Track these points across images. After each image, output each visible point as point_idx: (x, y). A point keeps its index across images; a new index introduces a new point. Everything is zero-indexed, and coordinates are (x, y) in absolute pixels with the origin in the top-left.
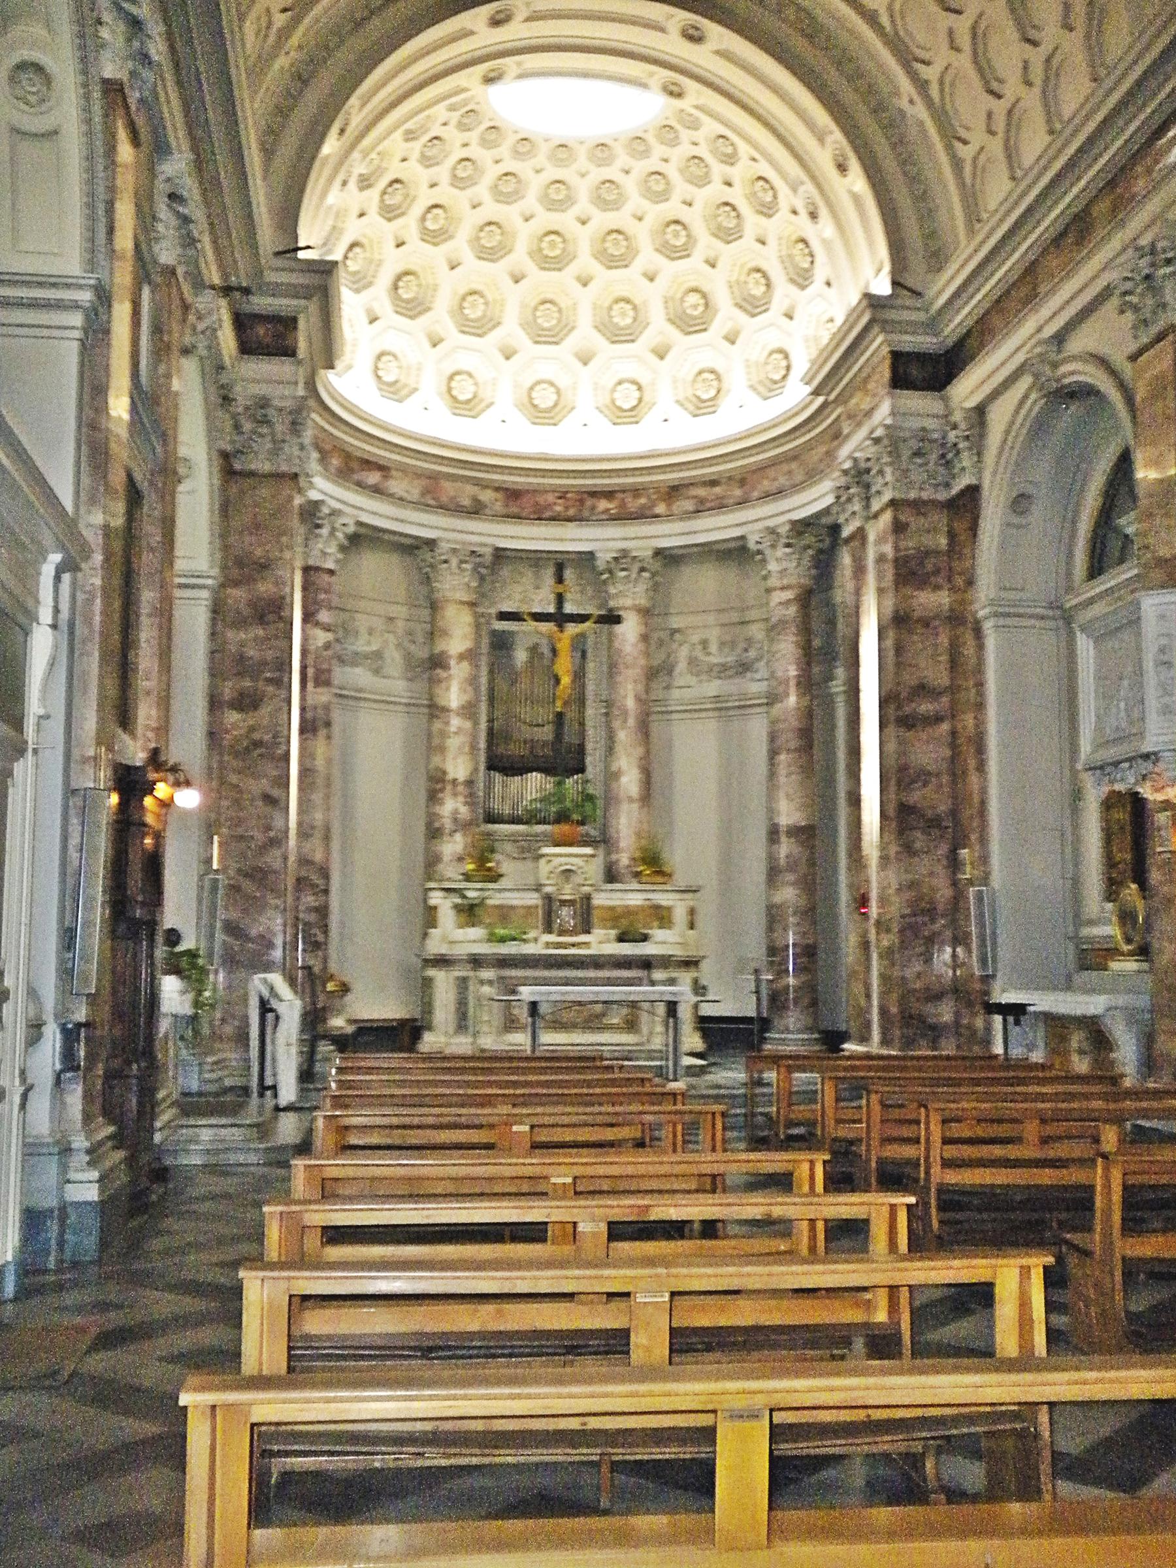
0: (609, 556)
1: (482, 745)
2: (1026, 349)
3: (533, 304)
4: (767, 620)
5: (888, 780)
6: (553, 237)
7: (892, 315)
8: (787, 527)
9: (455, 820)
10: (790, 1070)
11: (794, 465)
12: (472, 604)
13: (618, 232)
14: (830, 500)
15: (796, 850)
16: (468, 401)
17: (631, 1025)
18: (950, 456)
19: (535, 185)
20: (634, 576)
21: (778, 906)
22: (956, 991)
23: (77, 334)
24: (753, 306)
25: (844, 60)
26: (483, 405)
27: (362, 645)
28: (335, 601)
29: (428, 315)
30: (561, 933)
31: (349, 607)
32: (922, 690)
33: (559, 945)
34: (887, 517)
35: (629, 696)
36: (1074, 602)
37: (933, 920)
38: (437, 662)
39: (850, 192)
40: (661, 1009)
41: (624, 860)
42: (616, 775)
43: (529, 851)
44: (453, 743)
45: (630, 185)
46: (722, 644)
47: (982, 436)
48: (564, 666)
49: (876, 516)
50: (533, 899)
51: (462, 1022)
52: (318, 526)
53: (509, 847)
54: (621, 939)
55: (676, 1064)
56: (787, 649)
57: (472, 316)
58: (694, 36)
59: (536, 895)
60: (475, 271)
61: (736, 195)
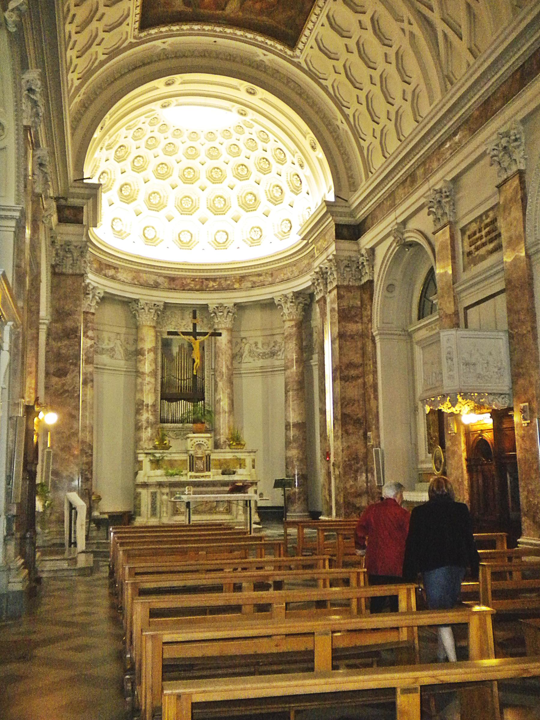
0: (214, 306)
1: (159, 389)
2: (391, 225)
3: (181, 198)
4: (283, 334)
5: (337, 404)
6: (189, 170)
7: (334, 209)
8: (292, 294)
9: (148, 422)
10: (303, 527)
11: (294, 268)
12: (154, 327)
13: (218, 168)
14: (310, 283)
15: (297, 433)
16: (153, 239)
17: (229, 511)
18: (360, 267)
19: (182, 148)
20: (225, 315)
21: (290, 458)
22: (367, 492)
23: (13, 229)
24: (275, 201)
25: (313, 104)
26: (159, 241)
27: (105, 345)
28: (96, 326)
29: (136, 202)
30: (197, 472)
31: (101, 329)
32: (351, 365)
33: (196, 477)
34: (335, 292)
35: (223, 366)
36: (412, 329)
37: (357, 463)
38: (139, 353)
39: (317, 158)
40: (241, 503)
41: (222, 438)
42: (219, 401)
43: (182, 435)
44: (146, 388)
45: (223, 149)
46: (263, 344)
47: (374, 260)
48: (196, 354)
49: (330, 292)
50: (185, 457)
51: (154, 512)
52: (88, 294)
53: (171, 434)
54: (223, 474)
55: (251, 527)
56: (292, 346)
57: (154, 203)
58: (252, 93)
59: (186, 455)
60: (155, 184)
61: (268, 155)
